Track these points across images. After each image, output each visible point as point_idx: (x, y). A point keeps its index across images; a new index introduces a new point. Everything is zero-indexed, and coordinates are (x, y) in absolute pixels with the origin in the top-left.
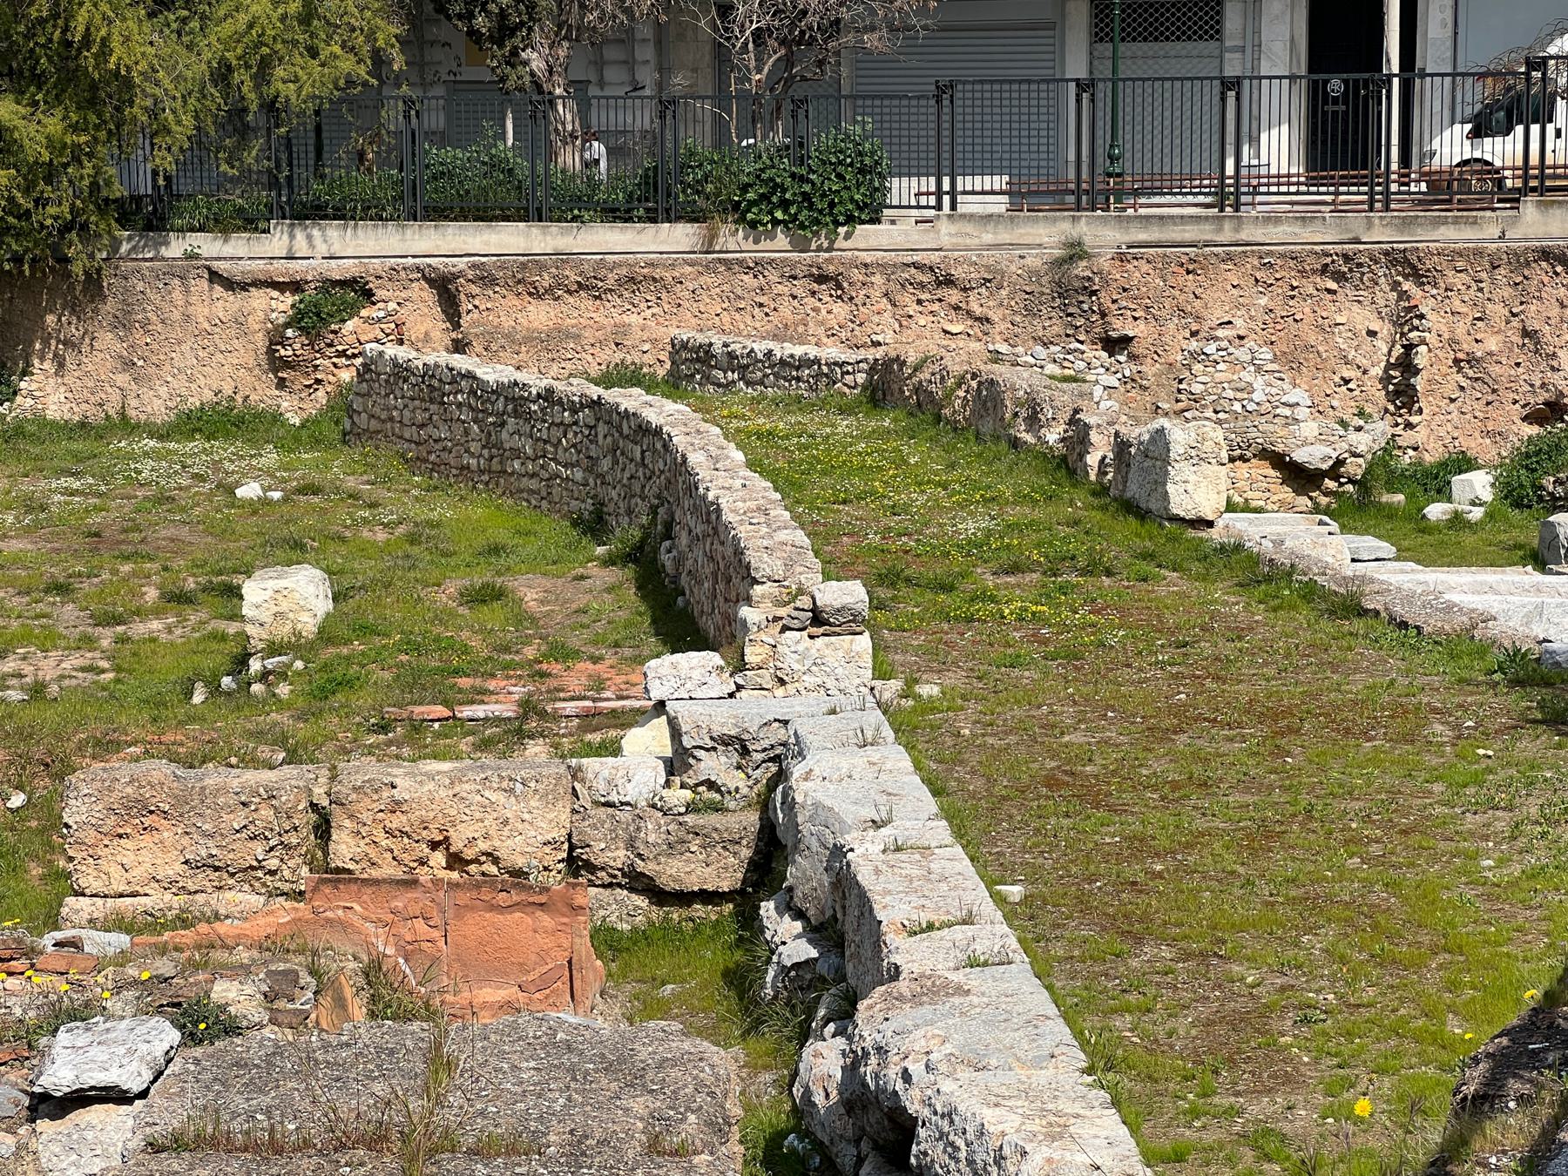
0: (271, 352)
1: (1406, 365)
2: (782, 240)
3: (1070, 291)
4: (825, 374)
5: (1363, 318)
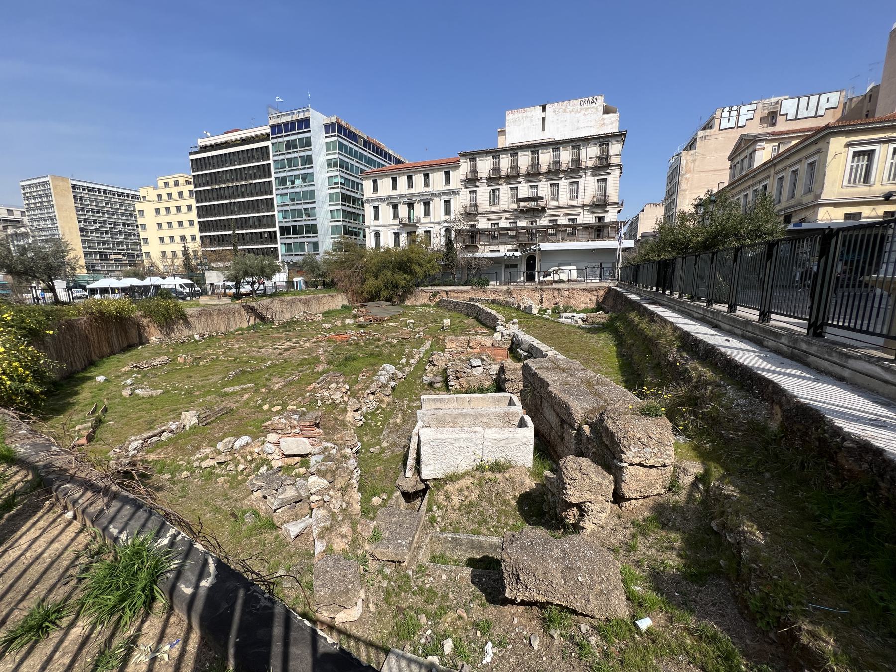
3: (509, 292)
4: (487, 300)
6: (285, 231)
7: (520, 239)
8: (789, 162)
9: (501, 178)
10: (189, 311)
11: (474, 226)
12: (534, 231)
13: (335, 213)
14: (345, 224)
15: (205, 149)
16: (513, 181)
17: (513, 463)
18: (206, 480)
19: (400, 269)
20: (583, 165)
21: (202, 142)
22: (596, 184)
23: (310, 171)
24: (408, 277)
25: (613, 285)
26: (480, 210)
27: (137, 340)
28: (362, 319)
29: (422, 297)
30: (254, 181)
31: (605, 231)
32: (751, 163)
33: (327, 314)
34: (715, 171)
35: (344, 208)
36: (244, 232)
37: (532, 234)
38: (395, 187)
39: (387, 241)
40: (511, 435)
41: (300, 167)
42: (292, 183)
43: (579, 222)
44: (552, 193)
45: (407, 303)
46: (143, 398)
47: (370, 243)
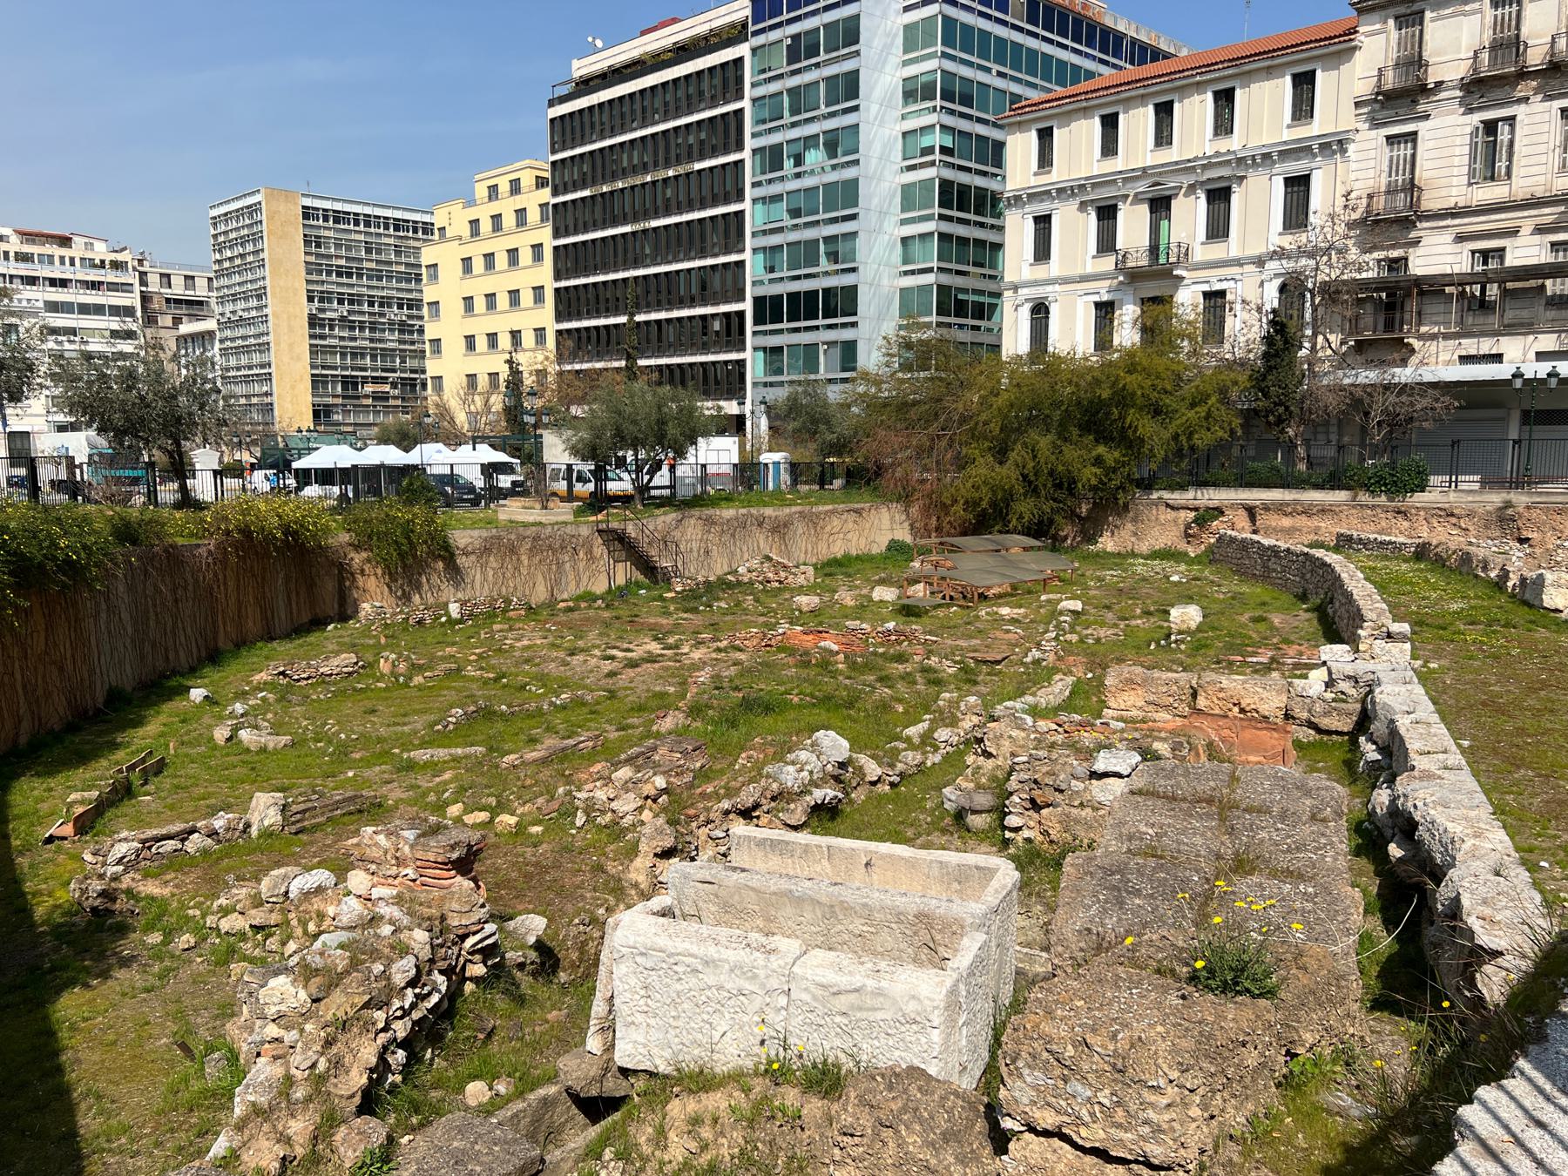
2: (1383, 498)
6: (768, 309)
9: (1523, 74)
10: (461, 538)
13: (916, 246)
14: (946, 279)
15: (587, 85)
18: (217, 964)
19: (1086, 428)
21: (583, 67)
23: (849, 119)
24: (1111, 455)
26: (1430, 202)
27: (331, 607)
28: (919, 590)
29: (1158, 526)
30: (698, 166)
33: (832, 568)
35: (947, 227)
36: (662, 315)
38: (1109, 147)
39: (1072, 334)
41: (824, 110)
42: (799, 160)
45: (1107, 543)
46: (248, 750)
47: (1015, 338)
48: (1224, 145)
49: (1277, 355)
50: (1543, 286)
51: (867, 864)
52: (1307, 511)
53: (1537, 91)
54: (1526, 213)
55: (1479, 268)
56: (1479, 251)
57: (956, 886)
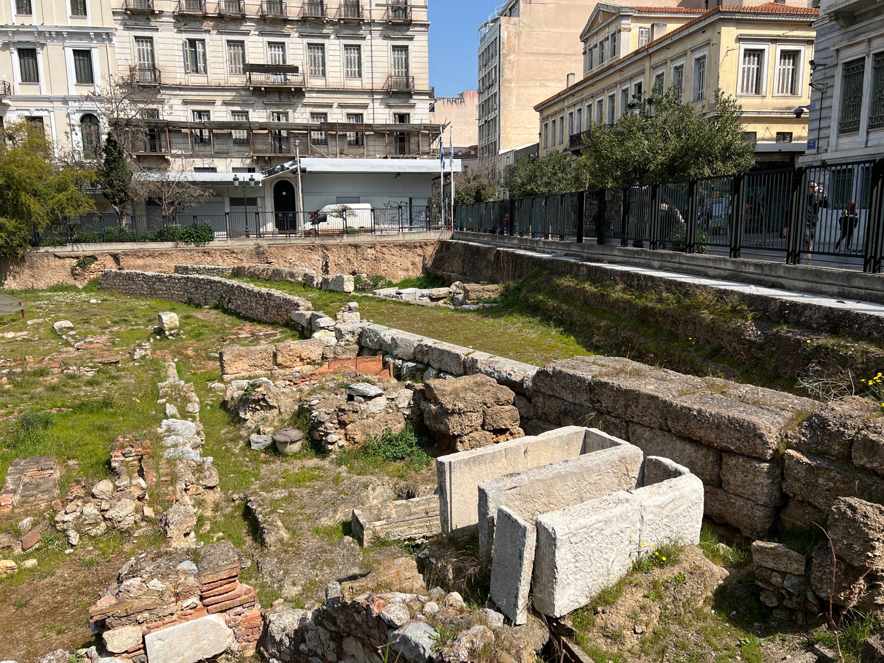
0: (72, 272)
1: (327, 265)
2: (193, 245)
5: (317, 257)
7: (259, 147)
8: (669, 54)
9: (205, 17)
11: (154, 113)
12: (284, 133)
16: (232, 27)
17: (681, 543)
20: (366, 16)
22: (390, 52)
25: (446, 236)
31: (413, 140)
32: (614, 51)
34: (547, 54)
37: (281, 138)
40: (677, 493)
43: (367, 120)
44: (313, 61)
48: (79, 23)
49: (114, 161)
50: (231, 133)
51: (525, 452)
52: (152, 255)
53: (214, 28)
54: (217, 94)
55: (198, 120)
56: (197, 111)
57: (566, 447)
